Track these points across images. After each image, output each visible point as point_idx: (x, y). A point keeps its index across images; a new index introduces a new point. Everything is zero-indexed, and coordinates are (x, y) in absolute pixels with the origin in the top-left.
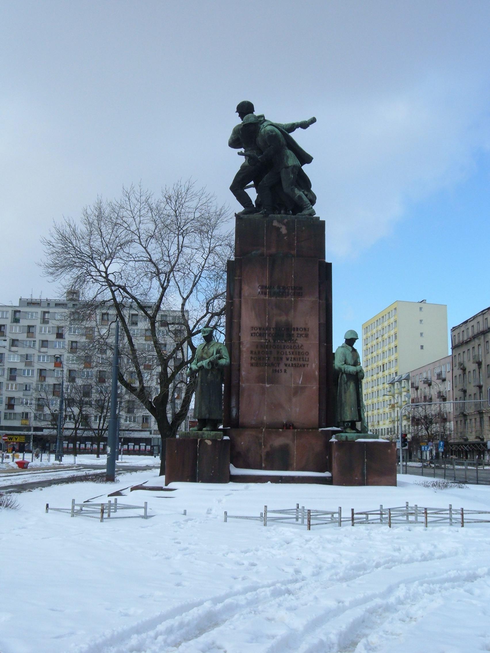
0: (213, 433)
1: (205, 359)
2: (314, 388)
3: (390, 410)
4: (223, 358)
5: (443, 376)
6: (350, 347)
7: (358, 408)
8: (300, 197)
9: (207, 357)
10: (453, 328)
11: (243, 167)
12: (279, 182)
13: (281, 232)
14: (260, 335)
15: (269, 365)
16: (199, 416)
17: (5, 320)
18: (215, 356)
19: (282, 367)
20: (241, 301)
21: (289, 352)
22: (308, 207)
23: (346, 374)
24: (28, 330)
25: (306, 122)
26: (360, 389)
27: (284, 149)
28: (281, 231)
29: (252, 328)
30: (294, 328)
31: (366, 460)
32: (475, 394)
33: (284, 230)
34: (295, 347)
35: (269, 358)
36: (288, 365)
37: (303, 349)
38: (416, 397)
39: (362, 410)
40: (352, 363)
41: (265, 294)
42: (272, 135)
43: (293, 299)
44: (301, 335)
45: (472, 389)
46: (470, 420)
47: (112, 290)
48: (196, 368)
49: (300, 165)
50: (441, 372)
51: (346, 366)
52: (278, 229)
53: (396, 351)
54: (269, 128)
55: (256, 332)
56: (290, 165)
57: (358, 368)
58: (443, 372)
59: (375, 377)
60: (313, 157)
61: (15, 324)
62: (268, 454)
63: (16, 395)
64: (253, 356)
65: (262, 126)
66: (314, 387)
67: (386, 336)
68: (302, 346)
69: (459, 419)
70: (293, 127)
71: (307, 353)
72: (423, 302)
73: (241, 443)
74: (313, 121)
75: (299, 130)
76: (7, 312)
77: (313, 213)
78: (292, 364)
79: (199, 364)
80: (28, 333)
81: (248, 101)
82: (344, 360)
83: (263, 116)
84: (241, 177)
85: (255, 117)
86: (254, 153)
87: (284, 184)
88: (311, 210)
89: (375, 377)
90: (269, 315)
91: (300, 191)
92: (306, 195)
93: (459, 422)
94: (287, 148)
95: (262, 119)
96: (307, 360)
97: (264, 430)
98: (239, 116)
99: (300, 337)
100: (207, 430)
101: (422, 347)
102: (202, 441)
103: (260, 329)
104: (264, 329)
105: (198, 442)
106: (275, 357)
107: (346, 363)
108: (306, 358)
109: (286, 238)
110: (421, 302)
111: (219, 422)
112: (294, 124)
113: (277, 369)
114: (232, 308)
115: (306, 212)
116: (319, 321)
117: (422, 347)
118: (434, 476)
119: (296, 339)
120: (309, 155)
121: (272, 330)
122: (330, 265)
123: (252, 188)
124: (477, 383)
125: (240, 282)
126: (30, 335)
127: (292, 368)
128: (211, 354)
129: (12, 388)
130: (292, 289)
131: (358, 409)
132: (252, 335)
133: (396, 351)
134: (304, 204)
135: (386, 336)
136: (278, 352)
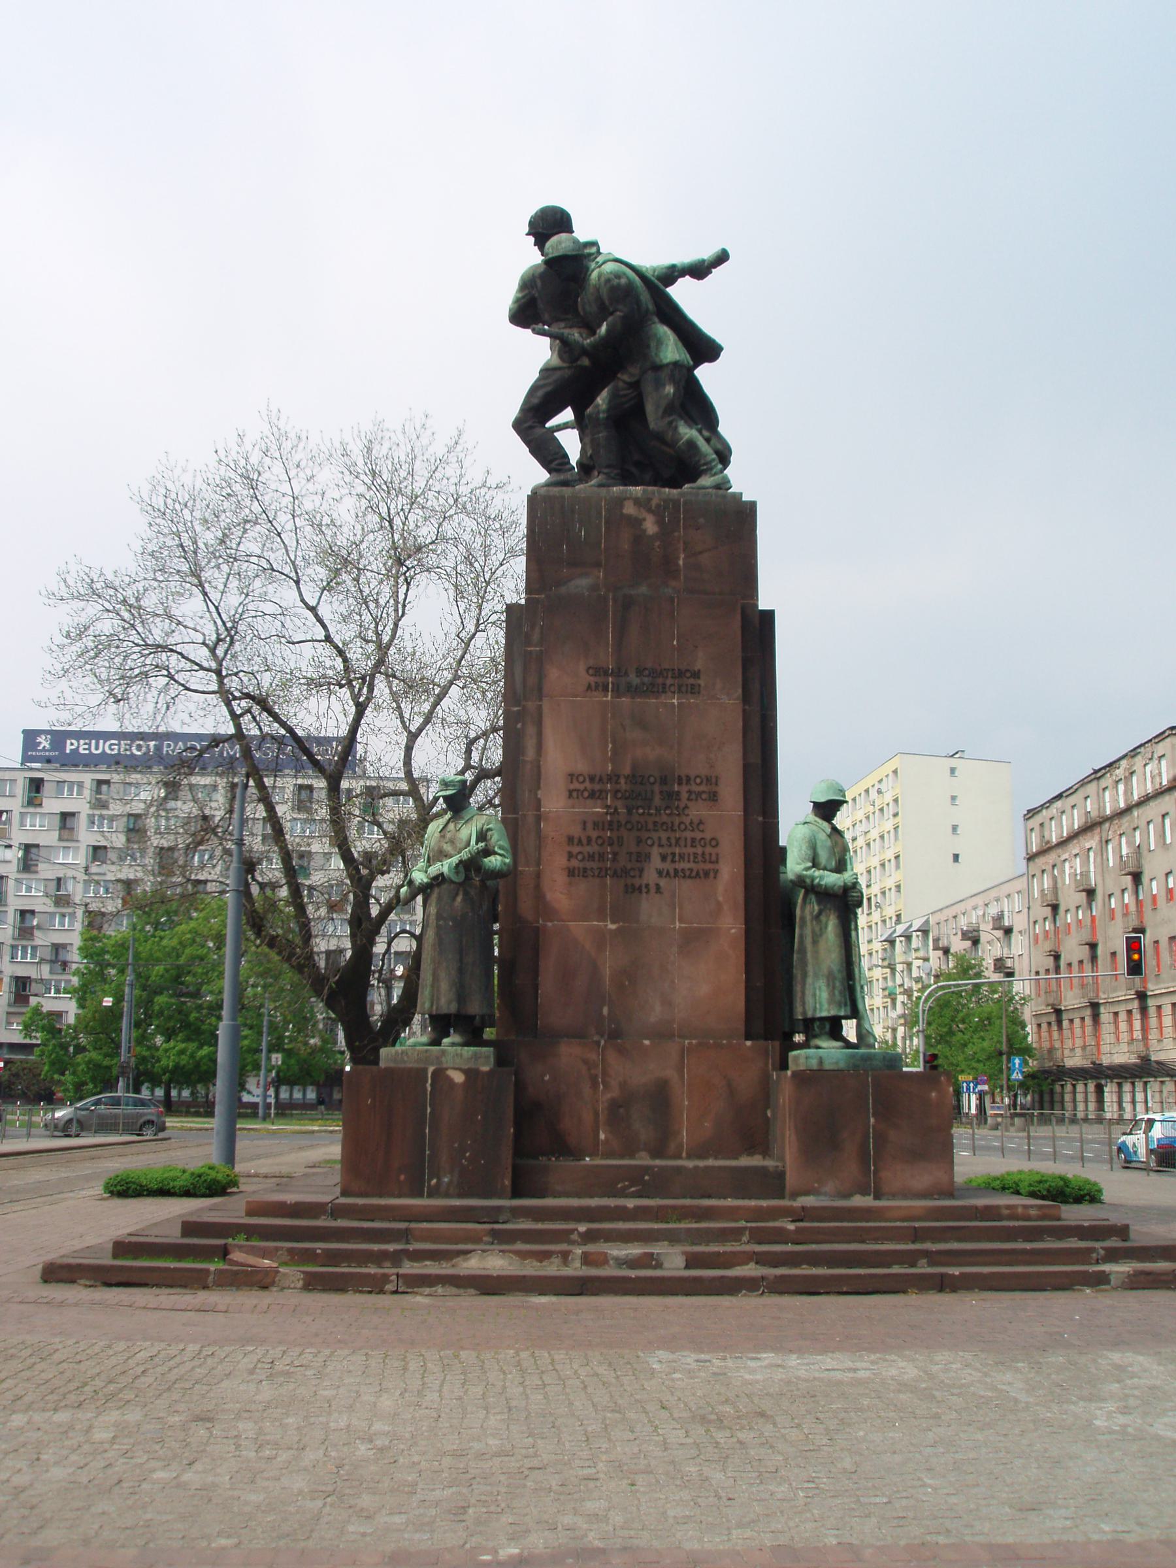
0: (469, 1051)
3: (885, 1000)
4: (495, 853)
5: (943, 943)
6: (825, 825)
8: (691, 444)
9: (453, 852)
10: (1029, 811)
11: (546, 371)
12: (638, 410)
13: (645, 531)
14: (593, 795)
15: (615, 874)
16: (432, 1006)
17: (9, 799)
18: (474, 846)
22: (711, 469)
24: (61, 821)
25: (703, 261)
26: (853, 933)
29: (572, 777)
30: (680, 778)
31: (872, 1120)
32: (1081, 962)
33: (650, 526)
34: (683, 827)
35: (615, 854)
36: (664, 874)
39: (858, 988)
42: (619, 284)
43: (675, 701)
44: (699, 794)
45: (1073, 950)
46: (1071, 1021)
47: (232, 713)
48: (425, 880)
49: (691, 363)
50: (1002, 912)
51: (817, 873)
52: (638, 522)
53: (898, 867)
54: (610, 267)
55: (581, 787)
56: (666, 361)
58: (1006, 913)
60: (723, 346)
61: (31, 810)
62: (615, 1106)
63: (32, 972)
64: (576, 849)
65: (593, 265)
68: (701, 822)
69: (1044, 1020)
70: (672, 275)
72: (957, 756)
73: (543, 1079)
74: (722, 258)
75: (686, 282)
76: (13, 781)
77: (724, 485)
78: (676, 870)
79: (433, 870)
80: (61, 829)
83: (594, 244)
84: (540, 393)
85: (576, 241)
90: (614, 742)
91: (691, 427)
92: (708, 440)
93: (1044, 1026)
94: (656, 320)
95: (594, 250)
96: (714, 858)
99: (696, 800)
100: (453, 1044)
101: (956, 858)
102: (439, 1074)
103: (592, 779)
104: (601, 780)
105: (430, 1075)
107: (815, 864)
108: (710, 854)
110: (952, 756)
111: (488, 1020)
112: (673, 267)
113: (637, 882)
114: (519, 726)
115: (706, 481)
117: (956, 858)
118: (1055, 1159)
121: (622, 781)
122: (768, 617)
123: (569, 430)
124: (1088, 939)
126: (66, 833)
128: (463, 845)
129: (24, 956)
132: (570, 796)
133: (898, 867)
135: (874, 834)
136: (639, 841)
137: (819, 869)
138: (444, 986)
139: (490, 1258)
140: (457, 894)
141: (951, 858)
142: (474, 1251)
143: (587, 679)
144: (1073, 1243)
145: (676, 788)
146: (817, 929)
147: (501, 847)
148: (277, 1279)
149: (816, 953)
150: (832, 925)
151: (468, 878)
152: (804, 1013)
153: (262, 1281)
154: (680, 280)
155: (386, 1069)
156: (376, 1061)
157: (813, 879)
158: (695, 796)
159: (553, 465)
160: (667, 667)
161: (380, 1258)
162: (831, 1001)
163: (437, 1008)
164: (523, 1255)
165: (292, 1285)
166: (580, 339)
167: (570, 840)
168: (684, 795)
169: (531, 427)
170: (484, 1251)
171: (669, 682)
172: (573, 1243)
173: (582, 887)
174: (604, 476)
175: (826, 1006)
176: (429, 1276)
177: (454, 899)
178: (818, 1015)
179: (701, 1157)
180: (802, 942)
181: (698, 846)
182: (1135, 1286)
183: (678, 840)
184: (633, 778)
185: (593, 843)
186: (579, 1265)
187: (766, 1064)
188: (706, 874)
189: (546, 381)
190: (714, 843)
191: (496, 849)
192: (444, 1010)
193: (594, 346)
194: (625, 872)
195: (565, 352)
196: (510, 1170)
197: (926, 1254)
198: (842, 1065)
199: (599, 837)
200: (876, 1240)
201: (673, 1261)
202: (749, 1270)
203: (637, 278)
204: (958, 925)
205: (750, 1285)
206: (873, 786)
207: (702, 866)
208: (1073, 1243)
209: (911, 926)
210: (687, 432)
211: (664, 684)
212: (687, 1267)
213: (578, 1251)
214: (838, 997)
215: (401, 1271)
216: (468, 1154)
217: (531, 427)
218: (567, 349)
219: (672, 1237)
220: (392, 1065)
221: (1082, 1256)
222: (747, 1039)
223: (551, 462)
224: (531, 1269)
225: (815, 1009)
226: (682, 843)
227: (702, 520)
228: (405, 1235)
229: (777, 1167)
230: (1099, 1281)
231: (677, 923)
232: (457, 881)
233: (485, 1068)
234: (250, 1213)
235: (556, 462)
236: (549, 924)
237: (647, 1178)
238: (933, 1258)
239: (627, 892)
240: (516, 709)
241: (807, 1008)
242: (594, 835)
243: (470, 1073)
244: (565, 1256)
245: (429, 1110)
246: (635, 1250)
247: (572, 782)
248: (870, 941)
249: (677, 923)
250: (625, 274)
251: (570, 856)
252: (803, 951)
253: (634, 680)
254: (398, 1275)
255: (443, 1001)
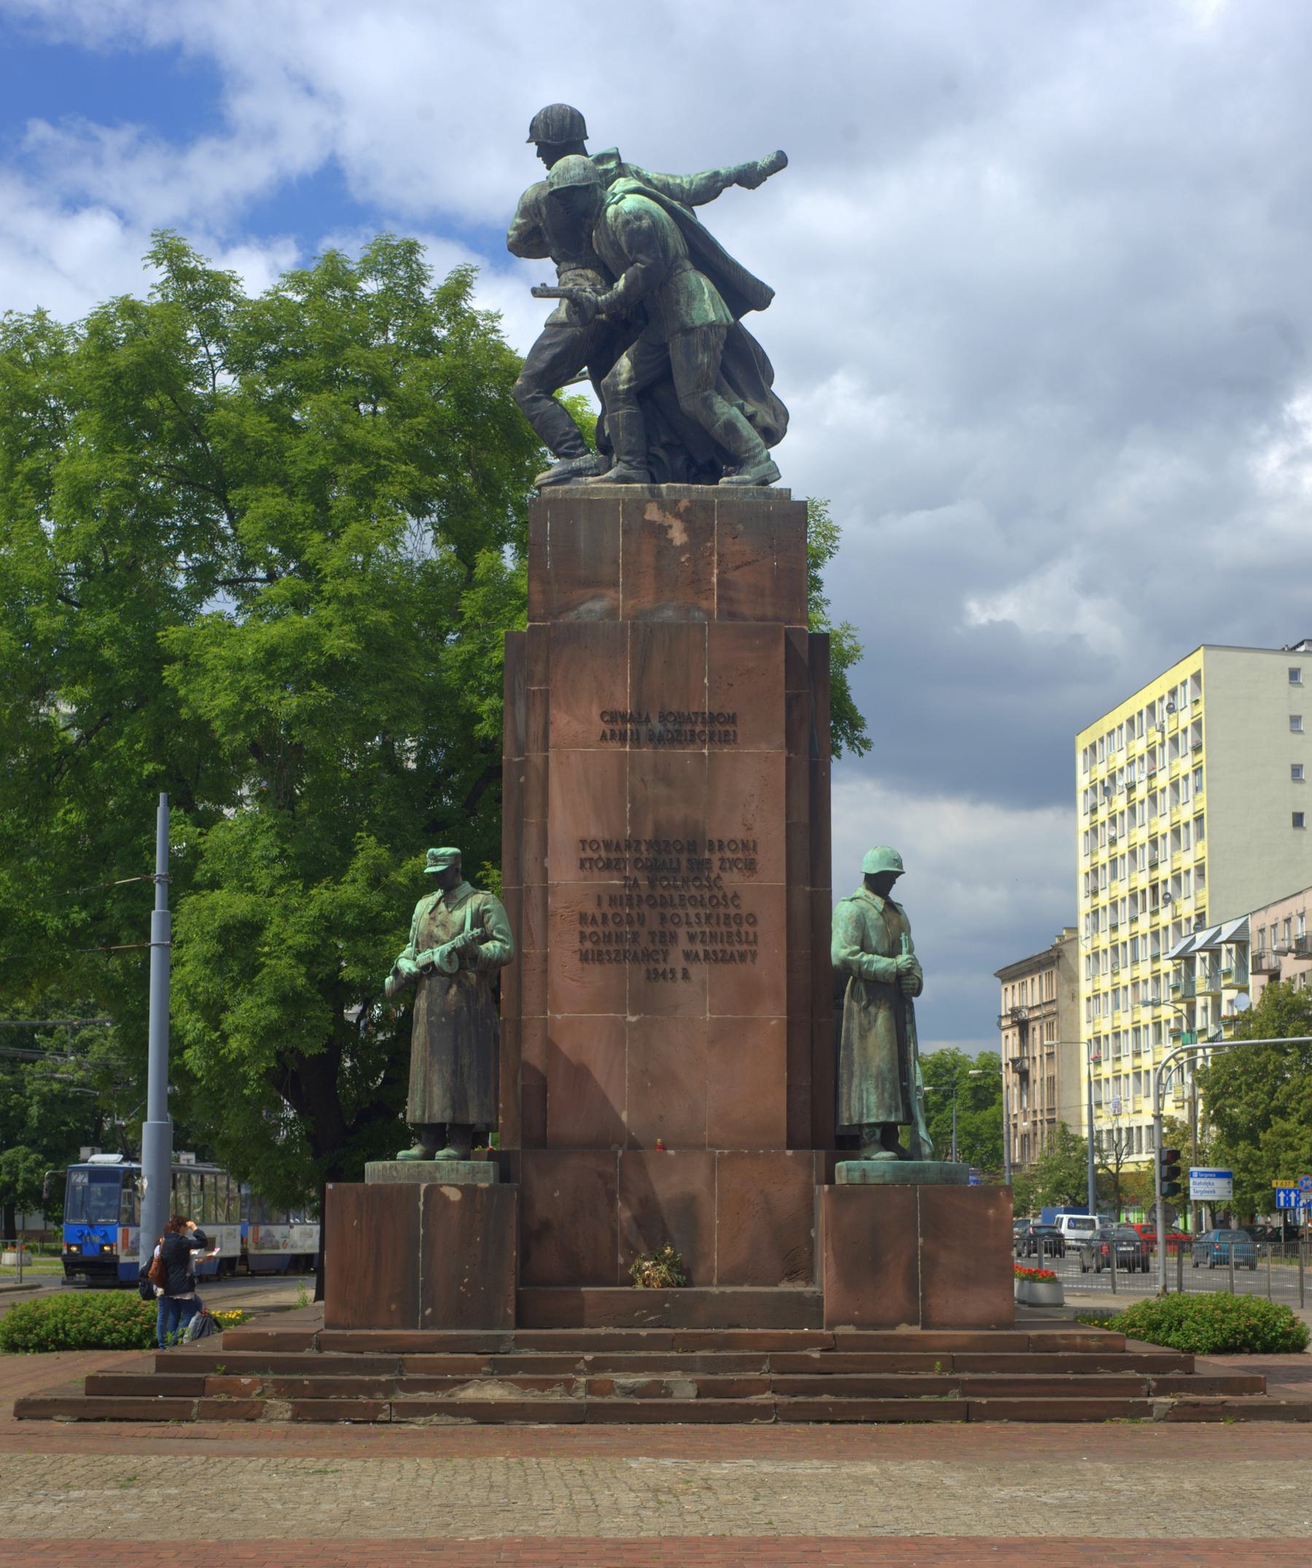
0: (464, 1165)
1: (440, 942)
2: (773, 1023)
7: (901, 1082)
8: (731, 427)
9: (445, 938)
13: (672, 540)
14: (608, 865)
15: (635, 958)
16: (424, 1113)
18: (469, 932)
19: (676, 959)
20: (547, 757)
21: (697, 915)
22: (755, 457)
23: (866, 981)
26: (909, 1027)
27: (678, 271)
28: (669, 537)
30: (711, 842)
31: (920, 1240)
33: (678, 535)
34: (715, 901)
35: (635, 934)
37: (737, 906)
38: (238, 1253)
40: (885, 946)
41: (623, 738)
42: (640, 227)
43: (706, 751)
44: (734, 862)
48: (414, 970)
51: (866, 958)
55: (595, 856)
57: (902, 959)
59: (1123, 934)
60: (774, 290)
64: (589, 929)
66: (771, 1019)
67: (1162, 780)
68: (736, 896)
71: (752, 919)
72: (1302, 649)
74: (780, 162)
77: (774, 473)
79: (423, 958)
81: (561, 106)
82: (859, 939)
84: (547, 355)
86: (585, 283)
87: (682, 384)
88: (767, 464)
89: (1123, 934)
90: (633, 801)
92: (751, 418)
94: (688, 265)
96: (751, 938)
97: (620, 1153)
98: (538, 155)
100: (449, 1158)
101: (1298, 819)
102: (433, 1190)
103: (608, 845)
104: (618, 846)
105: (422, 1192)
106: (654, 932)
107: (864, 947)
109: (688, 560)
112: (716, 174)
113: (661, 967)
114: (522, 779)
116: (787, 819)
119: (719, 877)
120: (763, 284)
121: (643, 847)
125: (546, 696)
127: (706, 966)
128: (457, 928)
130: (704, 723)
131: (901, 1086)
132: (582, 866)
134: (744, 449)
136: (663, 919)
137: (868, 953)
138: (437, 1091)
139: (488, 1387)
140: (450, 987)
141: (1289, 821)
142: (468, 1381)
143: (599, 726)
144: (1131, 1374)
145: (707, 855)
146: (865, 1022)
147: (500, 931)
148: (264, 1411)
149: (864, 1049)
150: (882, 1019)
151: (462, 968)
152: (850, 1118)
153: (250, 1414)
154: (726, 191)
155: (373, 1186)
156: (360, 1176)
157: (860, 964)
158: (726, 865)
159: (562, 449)
160: (696, 710)
161: (370, 1389)
162: (880, 1104)
163: (429, 1117)
164: (524, 1384)
165: (281, 1416)
166: (592, 296)
167: (583, 918)
168: (716, 864)
169: (535, 400)
170: (482, 1380)
171: (698, 729)
172: (579, 1372)
173: (596, 973)
174: (624, 465)
175: (874, 1111)
176: (424, 1404)
177: (447, 992)
178: (865, 1121)
179: (732, 1283)
180: (848, 1038)
181: (733, 923)
182: (1180, 1418)
183: (708, 917)
184: (654, 844)
185: (610, 923)
186: (583, 1394)
187: (810, 1177)
188: (742, 957)
189: (554, 340)
190: (751, 920)
191: (494, 933)
192: (438, 1119)
193: (610, 304)
194: (648, 956)
195: (575, 313)
196: (513, 1297)
197: (956, 1383)
198: (888, 1178)
199: (615, 915)
200: (909, 1370)
201: (684, 1388)
202: (766, 1398)
203: (663, 213)
204: (1293, 933)
205: (763, 1413)
206: (1161, 699)
207: (738, 947)
208: (1131, 1374)
209: (1219, 933)
210: (726, 410)
211: (693, 732)
212: (698, 1396)
213: (583, 1379)
214: (887, 1101)
215: (393, 1399)
216: (466, 1280)
217: (535, 400)
218: (577, 309)
219: (686, 1366)
220: (381, 1182)
221: (1134, 1386)
222: (789, 1148)
223: (560, 444)
224: (532, 1397)
225: (861, 1115)
226: (713, 921)
227: (740, 527)
228: (399, 1367)
229: (814, 1292)
230: (1143, 1411)
231: (708, 1015)
232: (450, 971)
233: (484, 1185)
234: (226, 1347)
235: (566, 445)
236: (559, 1017)
237: (667, 1305)
238: (967, 1388)
239: (648, 978)
240: (517, 759)
241: (853, 1113)
242: (610, 912)
243: (469, 1191)
244: (569, 1386)
245: (422, 1232)
246: (643, 1379)
247: (584, 849)
248: (1155, 958)
249: (708, 1015)
250: (647, 212)
251: (583, 937)
252: (849, 1046)
253: (657, 726)
254: (391, 1404)
255: (436, 1108)
